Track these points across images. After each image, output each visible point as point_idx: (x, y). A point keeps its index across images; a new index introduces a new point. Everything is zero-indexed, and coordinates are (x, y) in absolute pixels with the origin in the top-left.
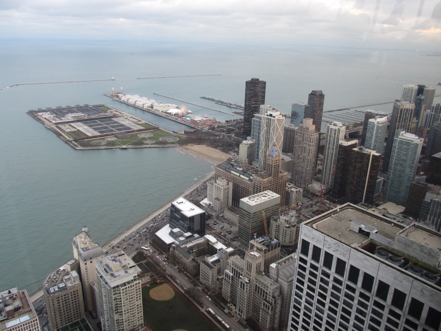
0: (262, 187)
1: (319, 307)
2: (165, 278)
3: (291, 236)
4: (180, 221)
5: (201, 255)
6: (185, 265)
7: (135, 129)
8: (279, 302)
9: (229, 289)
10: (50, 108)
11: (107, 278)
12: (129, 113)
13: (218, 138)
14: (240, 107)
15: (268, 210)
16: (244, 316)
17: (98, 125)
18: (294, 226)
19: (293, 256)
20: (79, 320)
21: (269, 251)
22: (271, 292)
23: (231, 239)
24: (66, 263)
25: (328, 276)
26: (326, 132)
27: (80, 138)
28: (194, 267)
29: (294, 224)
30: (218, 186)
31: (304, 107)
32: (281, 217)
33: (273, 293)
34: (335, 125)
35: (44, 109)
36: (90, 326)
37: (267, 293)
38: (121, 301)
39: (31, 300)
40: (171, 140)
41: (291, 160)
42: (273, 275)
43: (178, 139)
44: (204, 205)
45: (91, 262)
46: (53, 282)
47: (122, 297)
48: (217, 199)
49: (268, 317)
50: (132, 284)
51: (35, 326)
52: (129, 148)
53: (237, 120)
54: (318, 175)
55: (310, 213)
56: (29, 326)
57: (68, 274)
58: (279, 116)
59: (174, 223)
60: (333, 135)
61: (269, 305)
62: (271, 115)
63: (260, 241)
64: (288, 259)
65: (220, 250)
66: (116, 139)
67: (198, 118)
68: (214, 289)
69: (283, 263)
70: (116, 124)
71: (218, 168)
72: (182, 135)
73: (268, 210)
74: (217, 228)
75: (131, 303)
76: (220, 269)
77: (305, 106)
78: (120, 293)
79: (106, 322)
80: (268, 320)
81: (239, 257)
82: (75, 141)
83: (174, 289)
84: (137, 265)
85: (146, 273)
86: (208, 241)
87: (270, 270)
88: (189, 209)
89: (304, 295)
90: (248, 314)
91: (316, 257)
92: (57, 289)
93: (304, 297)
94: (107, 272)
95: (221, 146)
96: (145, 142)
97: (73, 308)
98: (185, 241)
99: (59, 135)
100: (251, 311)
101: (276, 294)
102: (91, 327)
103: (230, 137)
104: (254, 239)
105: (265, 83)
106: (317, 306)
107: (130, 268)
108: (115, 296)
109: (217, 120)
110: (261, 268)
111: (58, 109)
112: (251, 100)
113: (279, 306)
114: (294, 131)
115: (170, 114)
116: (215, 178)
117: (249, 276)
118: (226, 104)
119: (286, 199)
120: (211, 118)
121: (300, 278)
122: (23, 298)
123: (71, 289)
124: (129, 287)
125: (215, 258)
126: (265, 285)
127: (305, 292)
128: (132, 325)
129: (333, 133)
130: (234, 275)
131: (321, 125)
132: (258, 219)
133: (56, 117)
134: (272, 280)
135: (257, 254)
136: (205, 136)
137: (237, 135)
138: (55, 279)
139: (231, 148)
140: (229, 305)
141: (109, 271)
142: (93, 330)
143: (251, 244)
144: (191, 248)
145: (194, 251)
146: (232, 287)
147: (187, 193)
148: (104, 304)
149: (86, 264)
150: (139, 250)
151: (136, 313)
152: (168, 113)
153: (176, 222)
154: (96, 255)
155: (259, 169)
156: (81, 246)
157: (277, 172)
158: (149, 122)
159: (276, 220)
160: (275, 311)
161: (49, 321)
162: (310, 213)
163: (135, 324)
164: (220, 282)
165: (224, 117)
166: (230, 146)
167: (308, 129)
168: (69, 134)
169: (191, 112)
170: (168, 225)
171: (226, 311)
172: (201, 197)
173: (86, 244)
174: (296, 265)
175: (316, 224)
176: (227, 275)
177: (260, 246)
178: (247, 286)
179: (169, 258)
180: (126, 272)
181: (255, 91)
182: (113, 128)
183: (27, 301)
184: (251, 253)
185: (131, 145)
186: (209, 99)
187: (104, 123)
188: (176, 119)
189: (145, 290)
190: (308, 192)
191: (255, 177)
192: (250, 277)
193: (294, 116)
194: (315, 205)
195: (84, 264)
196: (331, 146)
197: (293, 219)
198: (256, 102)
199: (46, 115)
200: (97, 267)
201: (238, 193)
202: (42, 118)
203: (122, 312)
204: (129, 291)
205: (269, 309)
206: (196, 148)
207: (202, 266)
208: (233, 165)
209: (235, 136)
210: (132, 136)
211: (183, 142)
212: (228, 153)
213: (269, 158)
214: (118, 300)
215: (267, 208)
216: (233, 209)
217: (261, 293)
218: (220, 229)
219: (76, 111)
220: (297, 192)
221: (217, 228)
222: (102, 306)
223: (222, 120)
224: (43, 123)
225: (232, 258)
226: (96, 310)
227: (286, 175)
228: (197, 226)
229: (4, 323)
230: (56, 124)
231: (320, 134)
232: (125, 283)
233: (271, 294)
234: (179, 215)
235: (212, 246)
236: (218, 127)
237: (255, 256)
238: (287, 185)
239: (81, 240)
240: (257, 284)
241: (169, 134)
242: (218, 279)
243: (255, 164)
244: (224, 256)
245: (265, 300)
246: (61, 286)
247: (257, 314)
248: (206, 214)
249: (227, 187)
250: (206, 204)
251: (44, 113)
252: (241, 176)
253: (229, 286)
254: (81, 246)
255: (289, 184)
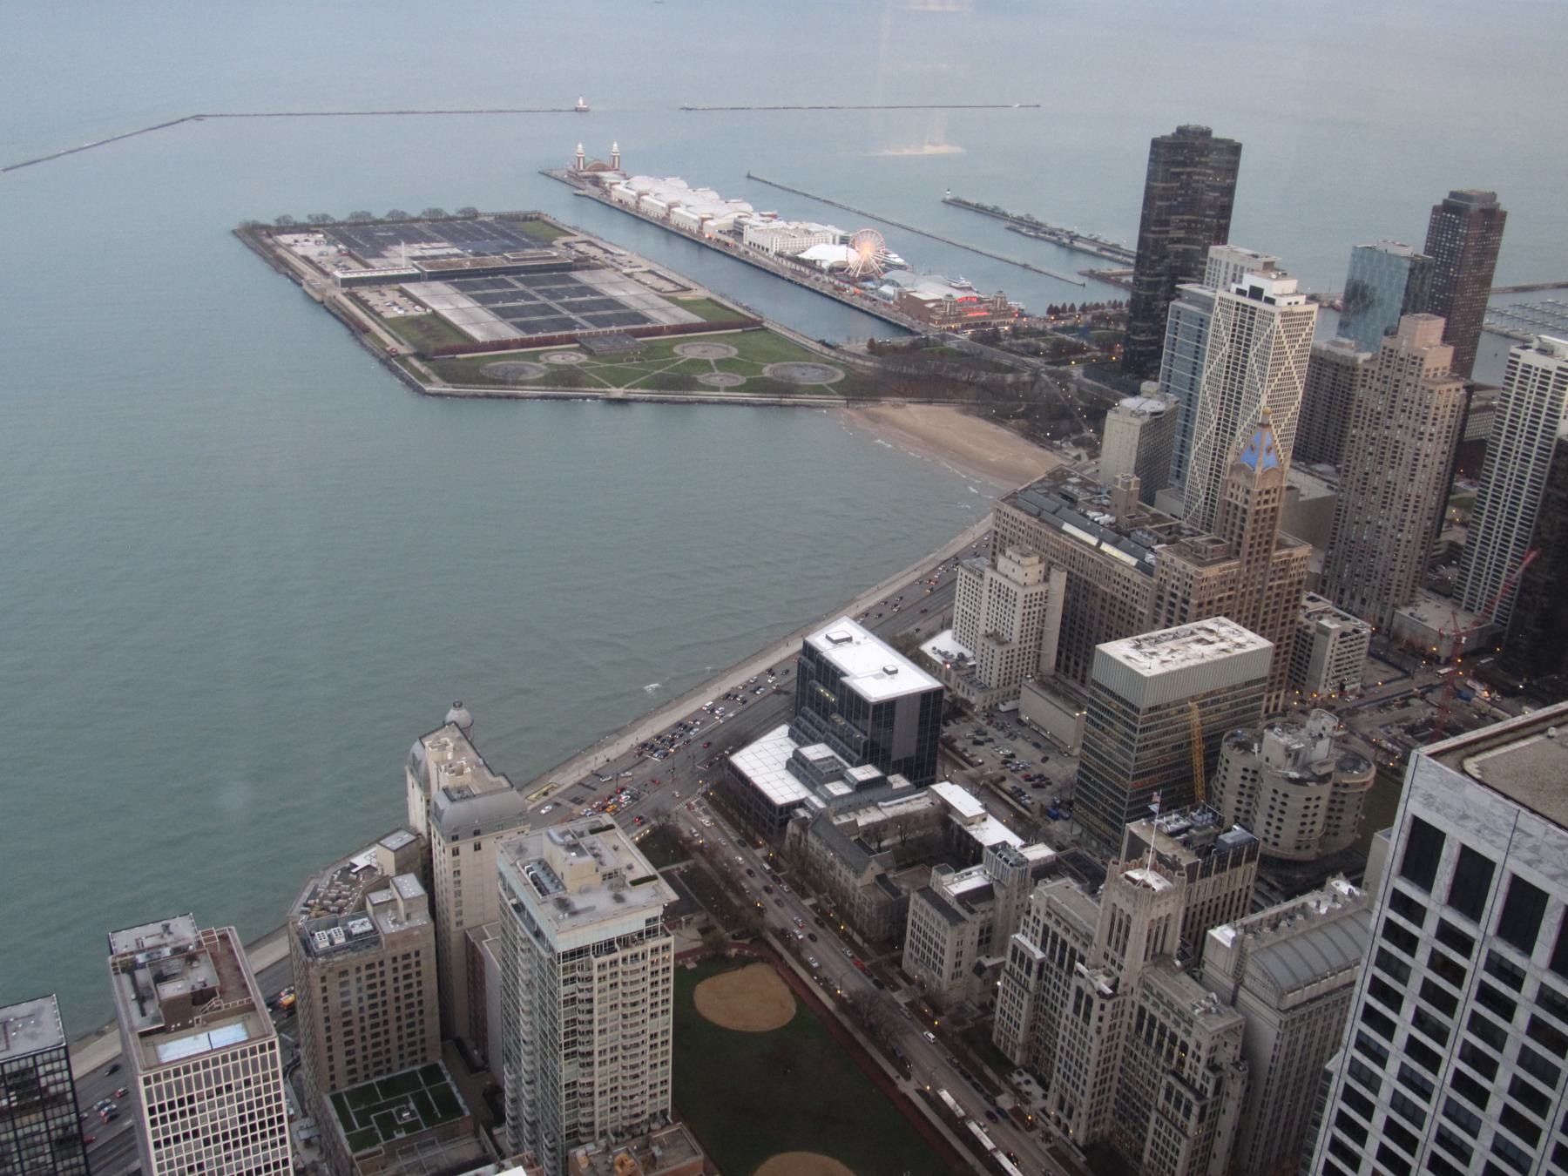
0: (1194, 601)
1: (1459, 1106)
2: (757, 939)
3: (1308, 820)
4: (835, 716)
5: (914, 864)
6: (845, 899)
7: (666, 321)
8: (1236, 1089)
9: (1023, 1012)
10: (325, 217)
11: (543, 913)
12: (639, 255)
13: (1010, 378)
14: (1115, 249)
15: (1214, 702)
16: (1079, 1132)
17: (515, 296)
18: (1322, 779)
19: (1313, 904)
20: (417, 1068)
21: (1206, 872)
22: (1206, 1043)
23: (1044, 811)
24: (378, 841)
25: (1515, 979)
26: (1499, 382)
27: (440, 345)
28: (882, 908)
29: (1324, 770)
30: (1004, 581)
31: (1407, 264)
32: (1269, 736)
33: (1213, 1049)
34: (1545, 351)
35: (301, 218)
36: (458, 1096)
37: (1184, 1048)
38: (590, 1011)
39: (255, 962)
40: (811, 376)
41: (1329, 493)
42: (1219, 976)
43: (840, 375)
44: (938, 659)
45: (477, 847)
46: (331, 913)
47: (596, 996)
48: (995, 637)
49: (1184, 1147)
50: (638, 949)
51: (265, 1067)
52: (636, 400)
53: (1097, 306)
54: (1443, 569)
55: (1395, 731)
56: (245, 1064)
57: (384, 884)
58: (1293, 299)
59: (811, 722)
60: (1531, 397)
61: (1191, 1096)
62: (1256, 293)
63: (1170, 828)
64: (1290, 915)
65: (994, 848)
66: (584, 358)
67: (929, 291)
68: (961, 1008)
69: (1266, 930)
70: (588, 298)
71: (1007, 508)
72: (859, 357)
73: (1214, 702)
74: (987, 759)
75: (627, 1022)
76: (989, 930)
77: (1413, 259)
78: (590, 979)
79: (525, 1088)
80: (1182, 1159)
81: (1075, 886)
82: (421, 356)
83: (793, 992)
84: (662, 874)
85: (684, 914)
86: (947, 807)
87: (1208, 953)
88: (874, 670)
89: (1396, 1050)
90: (1095, 1124)
91: (1468, 893)
92: (340, 940)
93: (1397, 1055)
94: (543, 891)
95: (1024, 416)
96: (701, 378)
97: (399, 1019)
98: (852, 800)
99: (357, 330)
100: (1109, 1115)
101: (1227, 1055)
102: (461, 1101)
103: (1065, 377)
104: (1150, 815)
105: (1235, 149)
106: (1449, 1099)
107: (635, 883)
108: (571, 988)
109: (1012, 303)
110: (1168, 942)
111: (356, 224)
112: (1167, 223)
113: (1231, 1108)
114: (1350, 368)
115: (811, 264)
116: (996, 546)
117: (1114, 969)
118: (1052, 233)
119: (1295, 657)
120: (987, 293)
121: (1387, 979)
122: (223, 956)
123: (393, 944)
124: (624, 960)
125: (973, 880)
126: (1180, 1013)
127: (1401, 1037)
128: (626, 1113)
129: (1533, 385)
130: (1052, 957)
131: (1475, 347)
132: (1167, 733)
133: (350, 254)
134: (1214, 996)
135: (1156, 881)
136: (957, 370)
137: (1093, 370)
138: (334, 900)
139: (1065, 425)
140: (1016, 1078)
141: (550, 887)
142: (467, 1113)
143: (1132, 834)
144: (875, 831)
145: (885, 843)
146: (1036, 1008)
147: (868, 602)
148: (523, 1017)
149: (456, 852)
150: (662, 819)
151: (646, 1067)
152: (804, 262)
153: (818, 718)
154: (498, 823)
155: (1184, 524)
156: (442, 780)
157: (1266, 544)
158: (723, 296)
159: (1245, 747)
160: (1213, 1125)
161: (304, 1062)
162: (1395, 731)
163: (638, 1110)
164: (986, 983)
165: (1043, 288)
166: (1066, 420)
167: (1417, 361)
168: (396, 326)
169: (899, 261)
170: (784, 729)
171: (1005, 1101)
172: (926, 626)
173: (461, 772)
174: (1375, 922)
175: (1479, 758)
176: (1019, 955)
177: (1169, 849)
178: (1102, 1007)
179: (782, 862)
180: (619, 899)
181: (1191, 185)
182: (574, 311)
183: (238, 969)
184: (1130, 873)
185: (647, 387)
186: (980, 209)
187: (540, 292)
188: (837, 288)
189: (686, 981)
190: (1393, 636)
191: (1167, 556)
192: (1118, 973)
193: (1357, 299)
194: (1423, 697)
195: (449, 851)
196: (1519, 445)
197: (1322, 749)
198: (1189, 230)
199: (308, 246)
200: (503, 869)
201: (1089, 616)
202: (295, 255)
203: (590, 1054)
204: (624, 973)
205: (1187, 1114)
206: (917, 415)
207: (918, 907)
208: (1072, 500)
209: (1086, 375)
210: (651, 350)
211: (860, 389)
212: (1052, 448)
213: (1234, 477)
214: (581, 1007)
215: (1212, 693)
216: (1058, 686)
217: (1160, 1044)
218: (997, 764)
219: (426, 231)
220: (1343, 635)
221: (987, 759)
222: (511, 1024)
223: (1029, 303)
224: (296, 279)
225: (1050, 889)
226: (485, 1039)
227: (1303, 555)
228: (904, 741)
229: (154, 1045)
230: (346, 283)
231: (1470, 389)
232: (611, 943)
233: (1203, 1055)
234: (833, 692)
235: (959, 828)
236: (1016, 332)
237: (1147, 886)
238: (1304, 602)
239: (441, 757)
240: (1148, 1006)
241: (805, 351)
242: (979, 969)
243: (1169, 504)
244: (1011, 876)
245: (1175, 1074)
246: (357, 930)
247: (1134, 1130)
248: (946, 696)
249: (1042, 588)
250: (945, 654)
251: (301, 237)
252: (1105, 547)
253: (1025, 1003)
254: (442, 780)
255: (1311, 599)
